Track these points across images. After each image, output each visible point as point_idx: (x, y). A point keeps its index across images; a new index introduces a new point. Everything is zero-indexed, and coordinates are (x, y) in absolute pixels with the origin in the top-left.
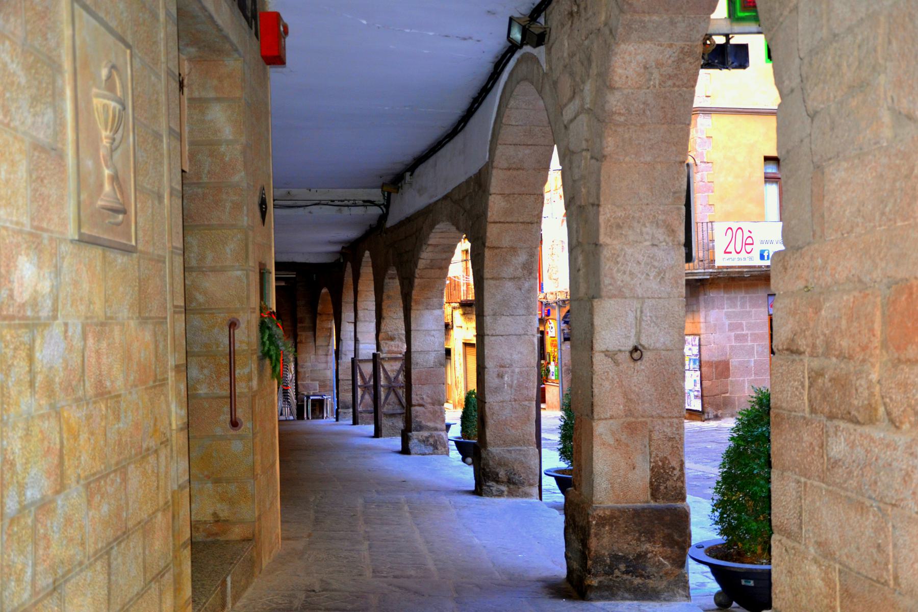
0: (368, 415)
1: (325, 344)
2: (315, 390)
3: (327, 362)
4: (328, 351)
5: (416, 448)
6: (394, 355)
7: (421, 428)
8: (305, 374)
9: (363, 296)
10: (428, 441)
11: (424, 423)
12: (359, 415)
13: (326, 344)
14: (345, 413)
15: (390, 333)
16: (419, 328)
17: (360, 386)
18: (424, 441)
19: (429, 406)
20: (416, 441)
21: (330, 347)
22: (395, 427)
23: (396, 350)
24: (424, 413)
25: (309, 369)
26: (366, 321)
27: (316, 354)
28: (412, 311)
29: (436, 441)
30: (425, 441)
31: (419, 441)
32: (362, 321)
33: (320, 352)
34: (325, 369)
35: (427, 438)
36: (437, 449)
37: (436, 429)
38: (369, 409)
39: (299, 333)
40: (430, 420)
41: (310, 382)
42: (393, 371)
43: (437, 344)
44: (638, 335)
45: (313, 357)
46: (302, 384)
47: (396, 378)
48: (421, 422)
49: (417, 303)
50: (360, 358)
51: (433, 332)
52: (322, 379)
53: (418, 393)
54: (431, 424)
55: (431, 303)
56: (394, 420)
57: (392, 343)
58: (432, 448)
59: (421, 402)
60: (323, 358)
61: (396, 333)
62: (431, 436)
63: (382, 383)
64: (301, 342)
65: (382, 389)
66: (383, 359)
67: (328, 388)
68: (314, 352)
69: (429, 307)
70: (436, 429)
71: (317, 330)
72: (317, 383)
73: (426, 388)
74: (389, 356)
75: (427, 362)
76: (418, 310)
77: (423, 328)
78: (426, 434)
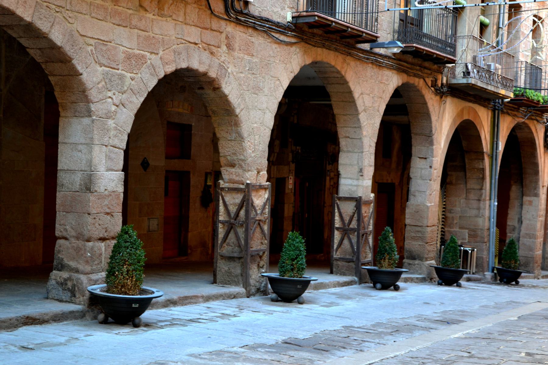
0: (344, 263)
1: (478, 187)
2: (463, 239)
3: (479, 209)
4: (481, 195)
5: (54, 291)
6: (236, 186)
7: (62, 267)
8: (453, 220)
9: (342, 121)
10: (66, 284)
11: (66, 261)
12: (335, 263)
13: (478, 187)
14: (410, 264)
15: (229, 158)
16: (66, 141)
17: (338, 229)
18: (62, 284)
19: (73, 240)
20: (53, 282)
21: (484, 191)
22: (230, 273)
23: (237, 179)
24: (68, 248)
25: (458, 215)
26: (349, 152)
27: (467, 198)
28: (60, 119)
29: (74, 286)
30: (63, 284)
31: (57, 283)
32: (344, 152)
33: (472, 196)
34: (477, 216)
35: (66, 280)
36: (75, 296)
37: (77, 271)
38: (348, 257)
39: (449, 173)
40: (73, 259)
41: (458, 230)
42: (234, 204)
43: (84, 162)
44: (122, 149)
45: (462, 201)
46: (449, 231)
47: (237, 214)
48: (62, 259)
49: (65, 109)
50: (341, 194)
51: (80, 147)
52: (472, 227)
53: (62, 222)
54: (73, 264)
55: (79, 109)
56: (232, 264)
57: (233, 170)
58: (69, 294)
59: (65, 234)
60: (474, 204)
61: (235, 158)
62: (70, 279)
63: (221, 218)
64: (451, 183)
65: (220, 226)
66: (222, 189)
67: (478, 239)
68: (464, 196)
69: (77, 114)
70: (77, 271)
71: (467, 171)
72: (466, 233)
73: (70, 216)
74: (232, 186)
75: (72, 184)
76: (66, 117)
77: (70, 141)
78: (65, 275)
